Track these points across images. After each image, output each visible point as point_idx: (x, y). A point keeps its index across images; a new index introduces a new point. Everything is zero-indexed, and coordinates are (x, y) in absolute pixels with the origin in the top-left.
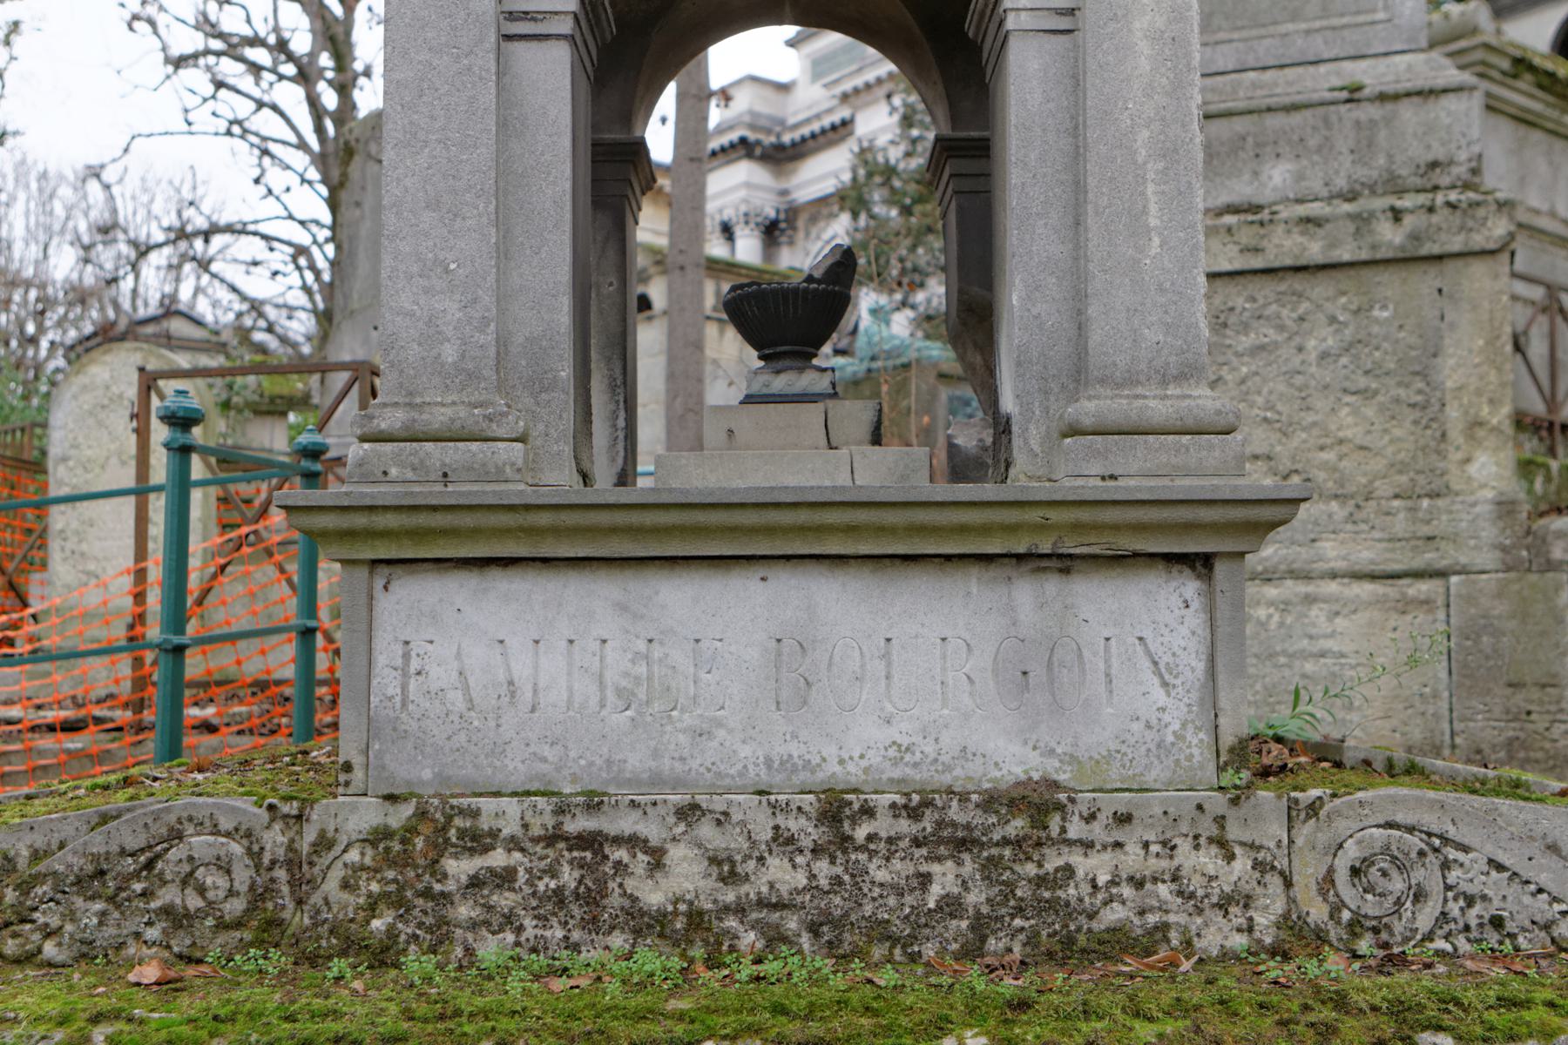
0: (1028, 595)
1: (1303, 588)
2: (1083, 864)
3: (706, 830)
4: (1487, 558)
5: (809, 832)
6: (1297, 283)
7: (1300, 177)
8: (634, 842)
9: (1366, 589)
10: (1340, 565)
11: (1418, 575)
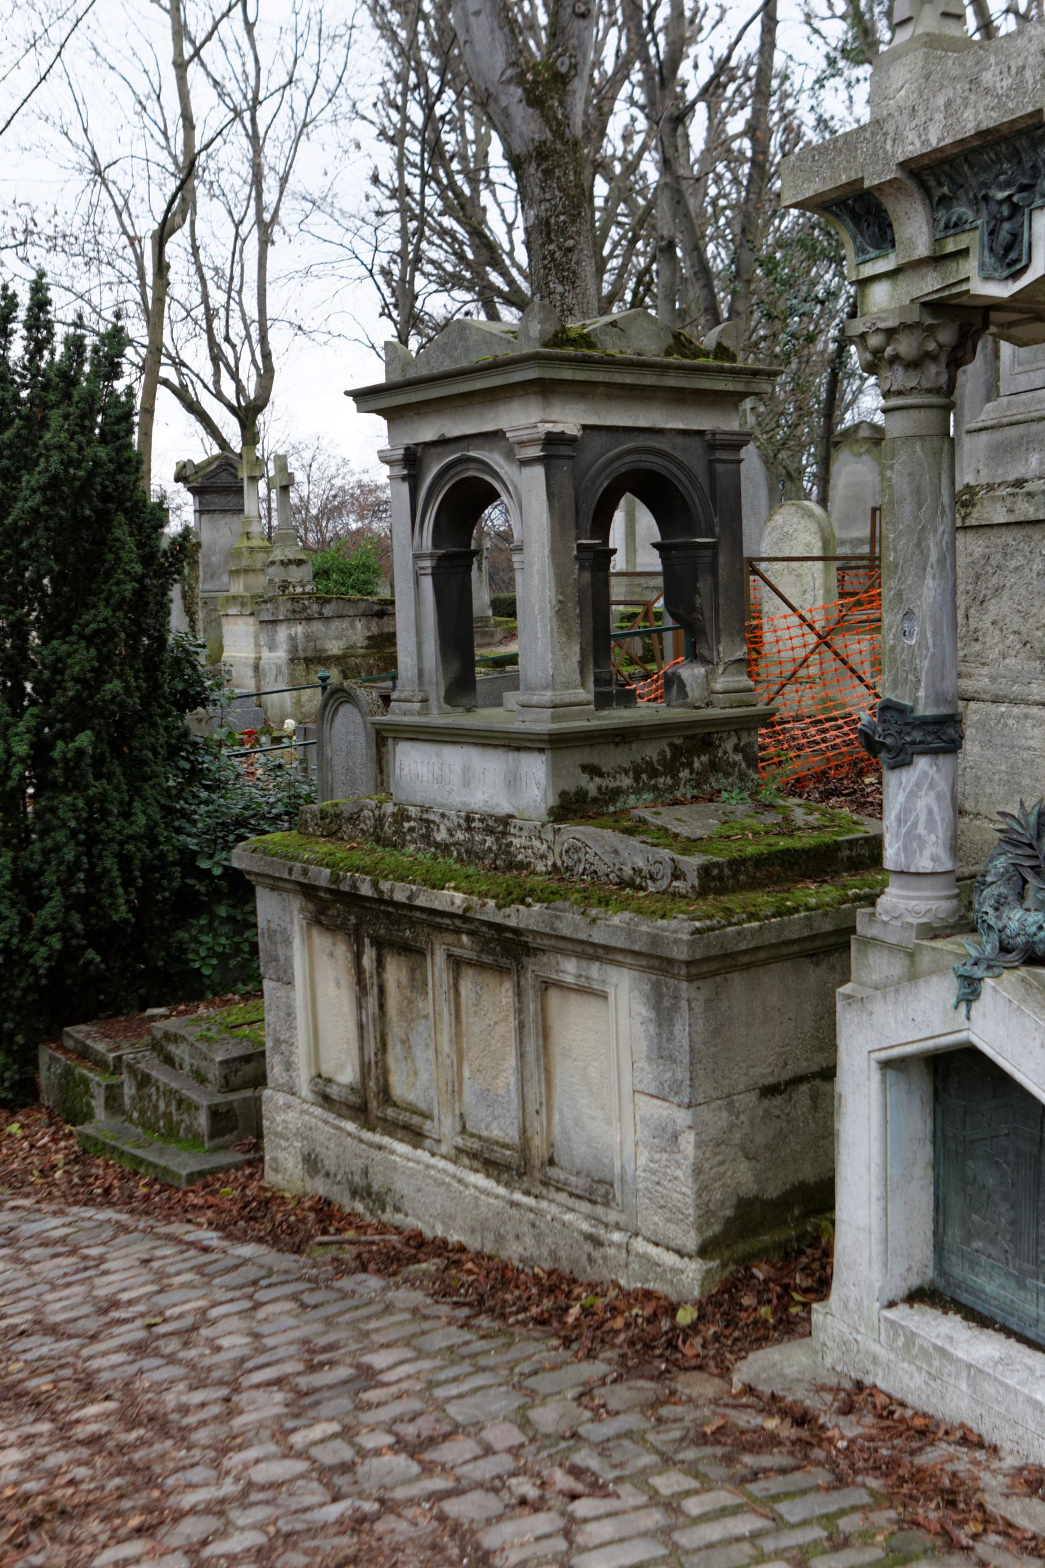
0: (511, 756)
5: (464, 825)
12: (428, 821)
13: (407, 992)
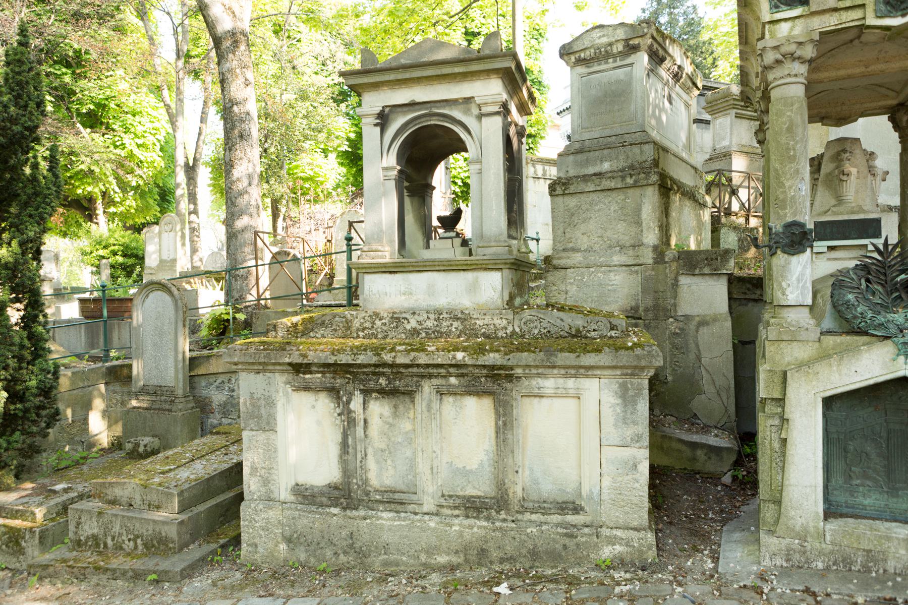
1: (609, 269)
2: (478, 322)
3: (416, 316)
4: (650, 261)
6: (609, 193)
7: (611, 166)
8: (405, 318)
9: (624, 268)
10: (617, 263)
11: (635, 265)
12: (397, 318)
13: (391, 420)
